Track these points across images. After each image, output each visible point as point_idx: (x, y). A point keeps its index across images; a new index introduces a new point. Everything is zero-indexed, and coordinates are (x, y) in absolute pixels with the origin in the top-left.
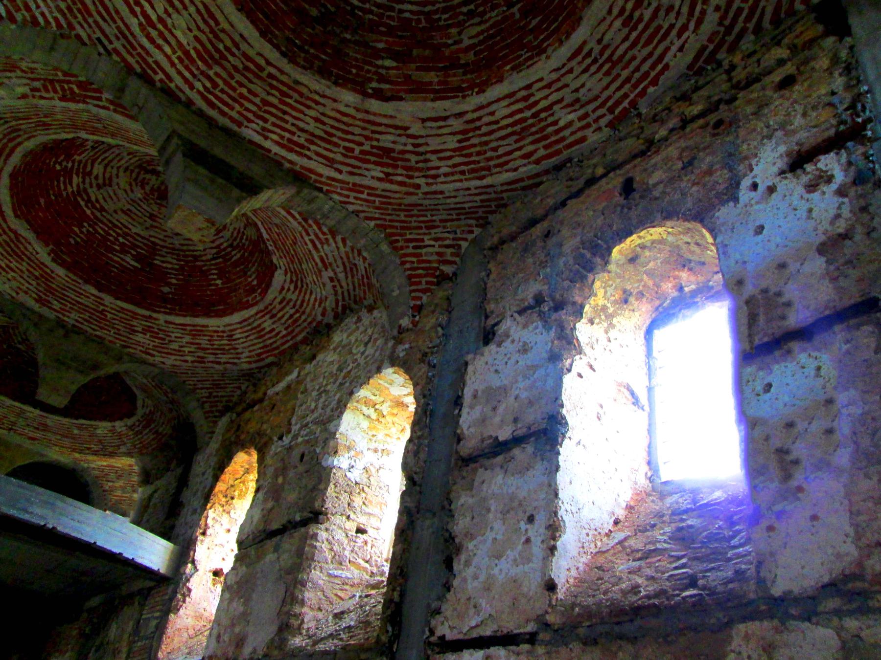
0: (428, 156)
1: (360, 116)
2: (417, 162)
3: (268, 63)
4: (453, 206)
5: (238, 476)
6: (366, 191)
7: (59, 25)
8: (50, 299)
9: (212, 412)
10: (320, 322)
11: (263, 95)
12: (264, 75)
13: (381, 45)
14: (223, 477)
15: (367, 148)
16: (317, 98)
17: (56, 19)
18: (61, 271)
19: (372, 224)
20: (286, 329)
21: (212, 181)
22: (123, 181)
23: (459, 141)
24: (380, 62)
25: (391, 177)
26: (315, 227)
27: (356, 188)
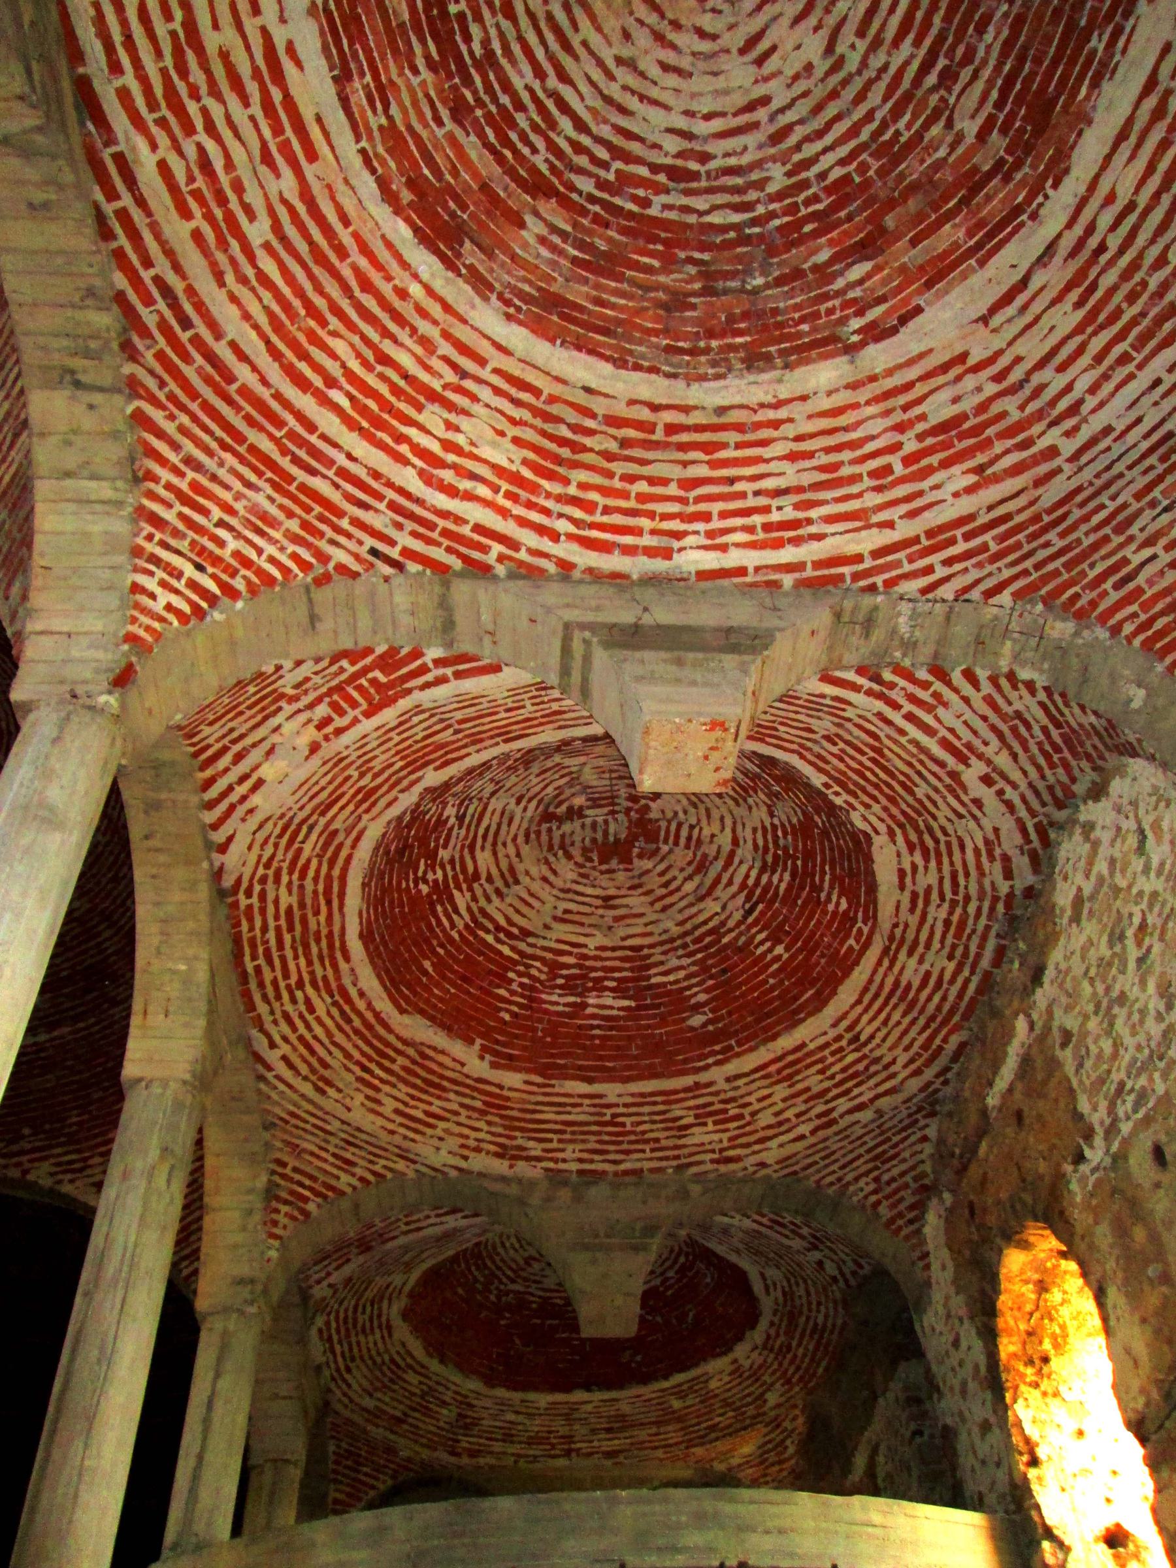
0: (1037, 379)
1: (863, 395)
2: (1022, 408)
3: (655, 408)
4: (1145, 445)
5: (1029, 1307)
6: (958, 533)
7: (305, 566)
8: (520, 1142)
9: (900, 1215)
10: (1010, 896)
11: (676, 472)
12: (659, 435)
13: (823, 256)
14: (1001, 1323)
15: (911, 446)
16: (771, 415)
17: (295, 557)
18: (513, 1079)
19: (1005, 598)
20: (950, 957)
21: (679, 662)
22: (530, 865)
23: (1078, 305)
24: (840, 283)
25: (989, 471)
26: (902, 683)
27: (939, 537)
